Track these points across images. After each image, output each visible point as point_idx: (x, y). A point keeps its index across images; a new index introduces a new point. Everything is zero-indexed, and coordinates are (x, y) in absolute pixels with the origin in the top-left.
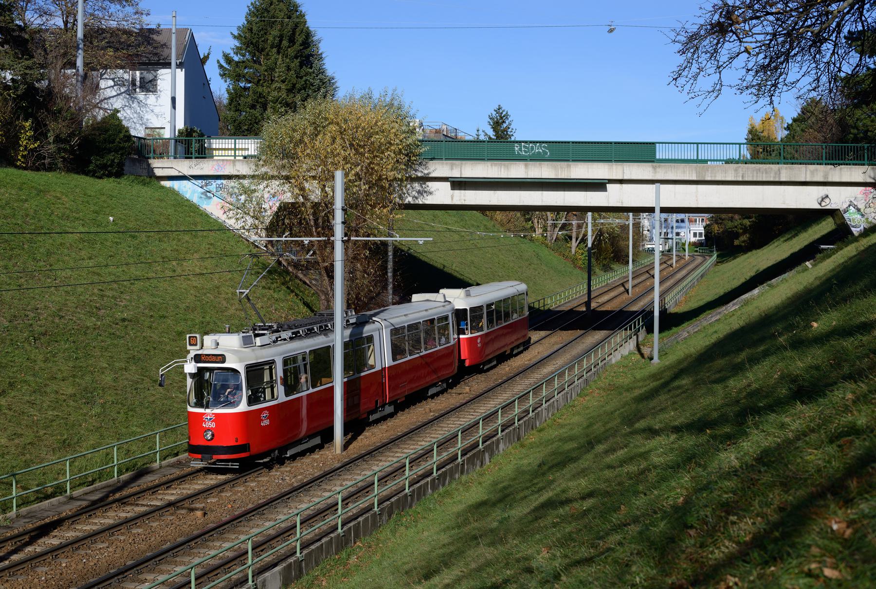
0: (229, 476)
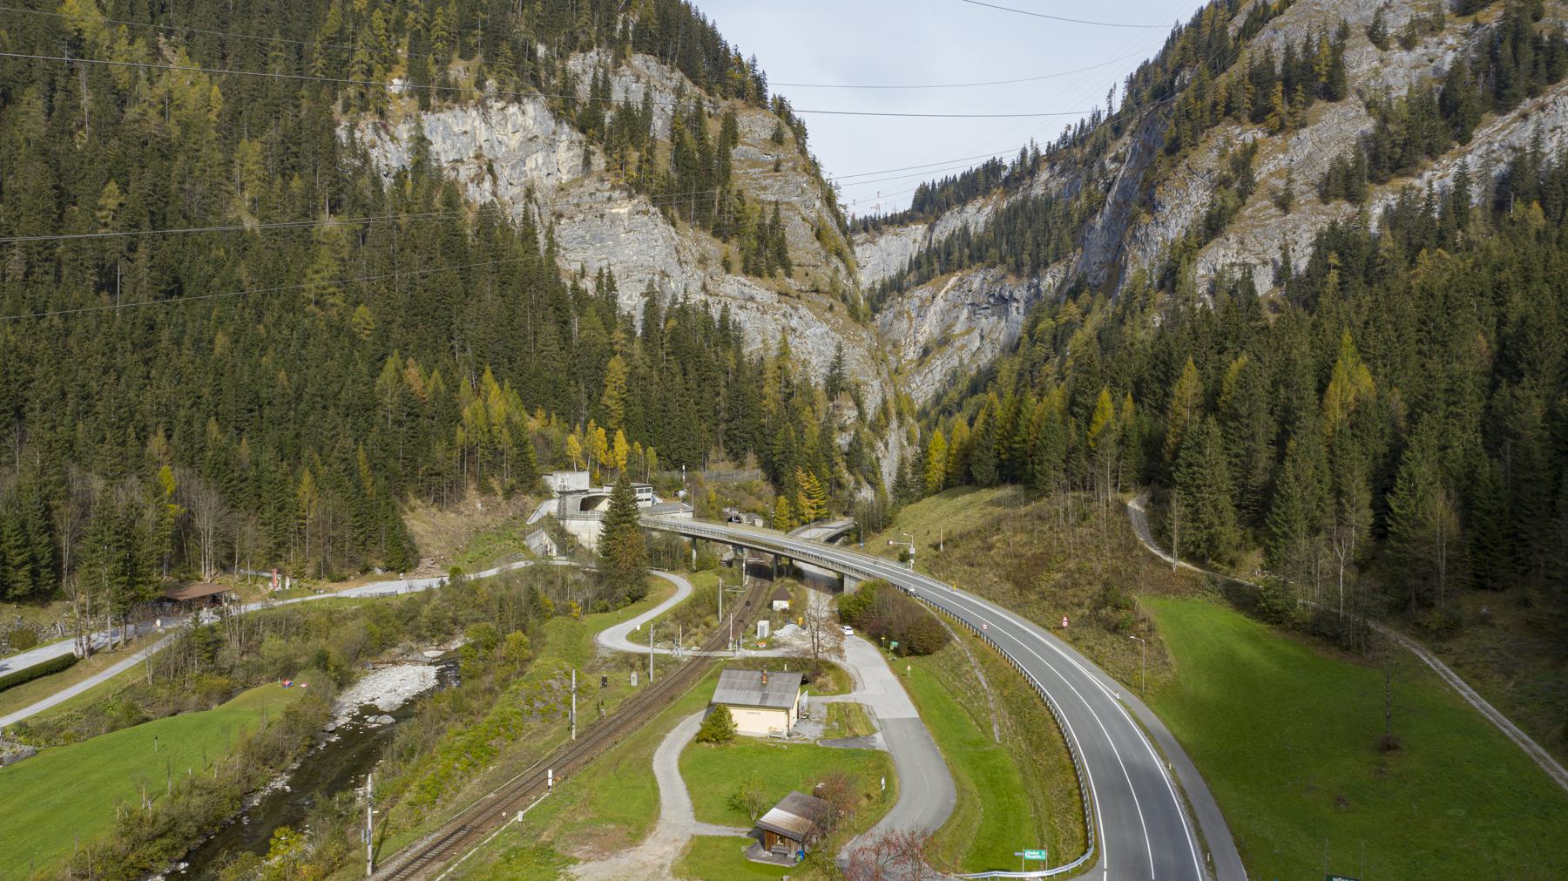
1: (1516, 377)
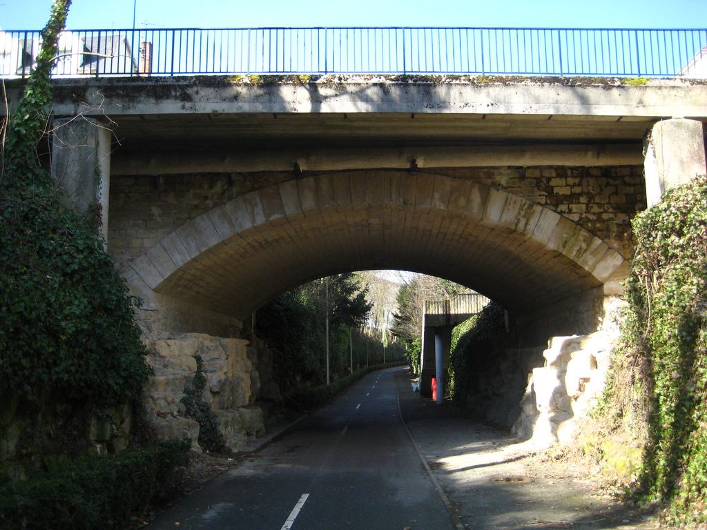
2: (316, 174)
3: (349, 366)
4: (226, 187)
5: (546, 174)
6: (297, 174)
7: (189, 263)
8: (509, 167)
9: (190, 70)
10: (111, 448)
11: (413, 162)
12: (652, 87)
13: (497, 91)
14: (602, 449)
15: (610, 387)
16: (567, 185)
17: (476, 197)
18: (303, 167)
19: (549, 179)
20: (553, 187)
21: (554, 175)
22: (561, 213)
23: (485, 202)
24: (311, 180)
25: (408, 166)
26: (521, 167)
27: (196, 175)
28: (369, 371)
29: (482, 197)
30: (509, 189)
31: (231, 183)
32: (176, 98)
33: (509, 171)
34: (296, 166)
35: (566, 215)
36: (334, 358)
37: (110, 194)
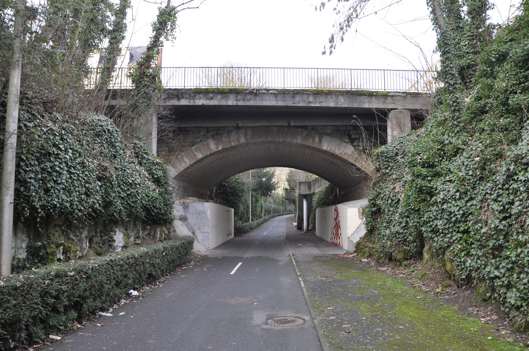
0: (394, 25)
1: (383, 235)
2: (246, 128)
3: (262, 213)
4: (206, 133)
5: (349, 128)
6: (238, 128)
7: (189, 166)
8: (332, 126)
9: (192, 85)
10: (13, 21)
11: (289, 123)
12: (390, 96)
13: (322, 98)
14: (313, 330)
15: (390, 219)
16: (358, 134)
17: (317, 140)
18: (240, 125)
19: (349, 131)
20: (351, 134)
21: (352, 129)
22: (354, 146)
23: (320, 141)
24: (244, 130)
25: (287, 124)
26: (337, 126)
27: (192, 127)
28: (273, 217)
29: (319, 139)
30: (331, 135)
31: (208, 131)
32: (187, 98)
33: (331, 127)
34: (237, 124)
35: (357, 147)
36: (254, 208)
37: (157, 143)
